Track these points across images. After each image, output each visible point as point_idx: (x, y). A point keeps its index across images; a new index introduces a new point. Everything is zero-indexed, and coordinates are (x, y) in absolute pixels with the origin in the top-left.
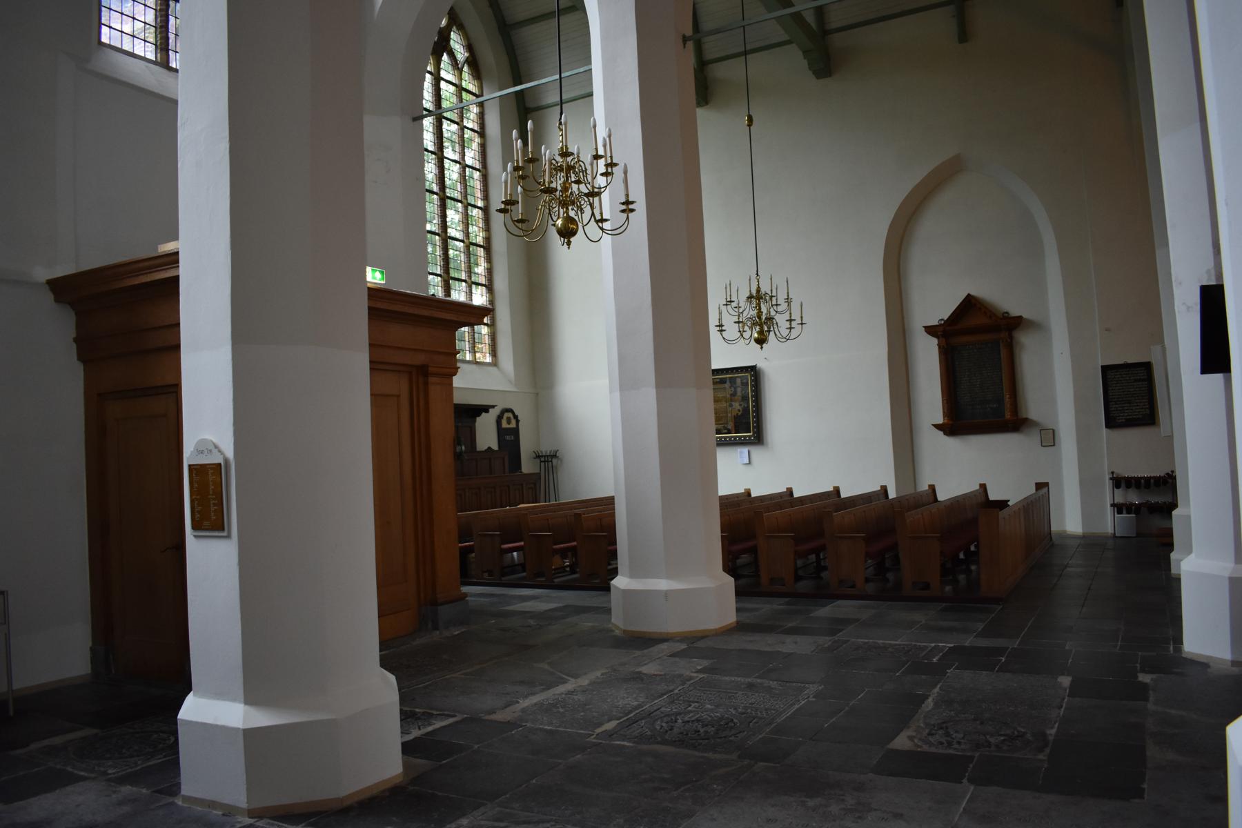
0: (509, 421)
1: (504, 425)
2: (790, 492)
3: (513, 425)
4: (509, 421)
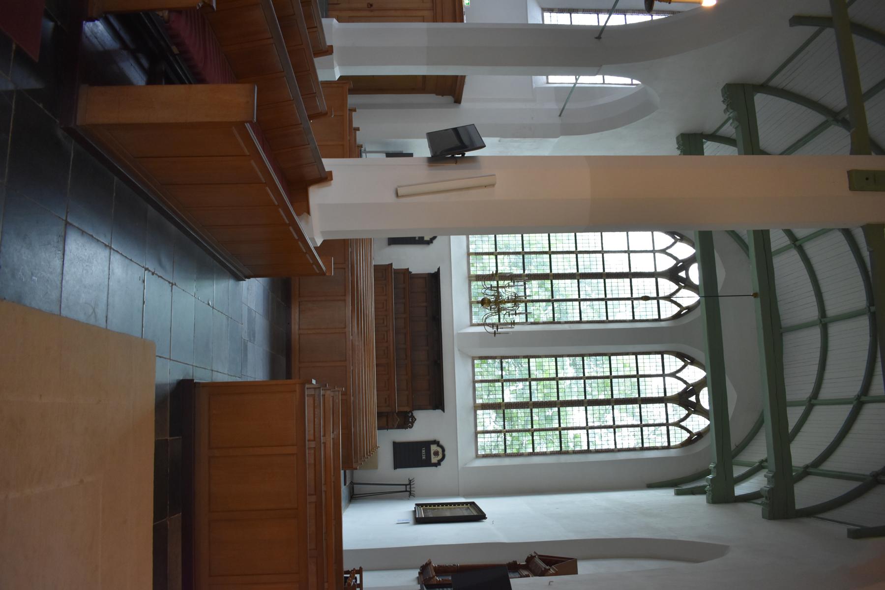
0: (436, 454)
1: (434, 448)
3: (434, 460)
4: (436, 454)
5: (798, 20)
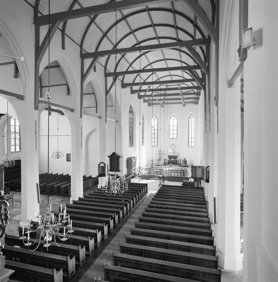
2: (57, 174)
5: (63, 48)
